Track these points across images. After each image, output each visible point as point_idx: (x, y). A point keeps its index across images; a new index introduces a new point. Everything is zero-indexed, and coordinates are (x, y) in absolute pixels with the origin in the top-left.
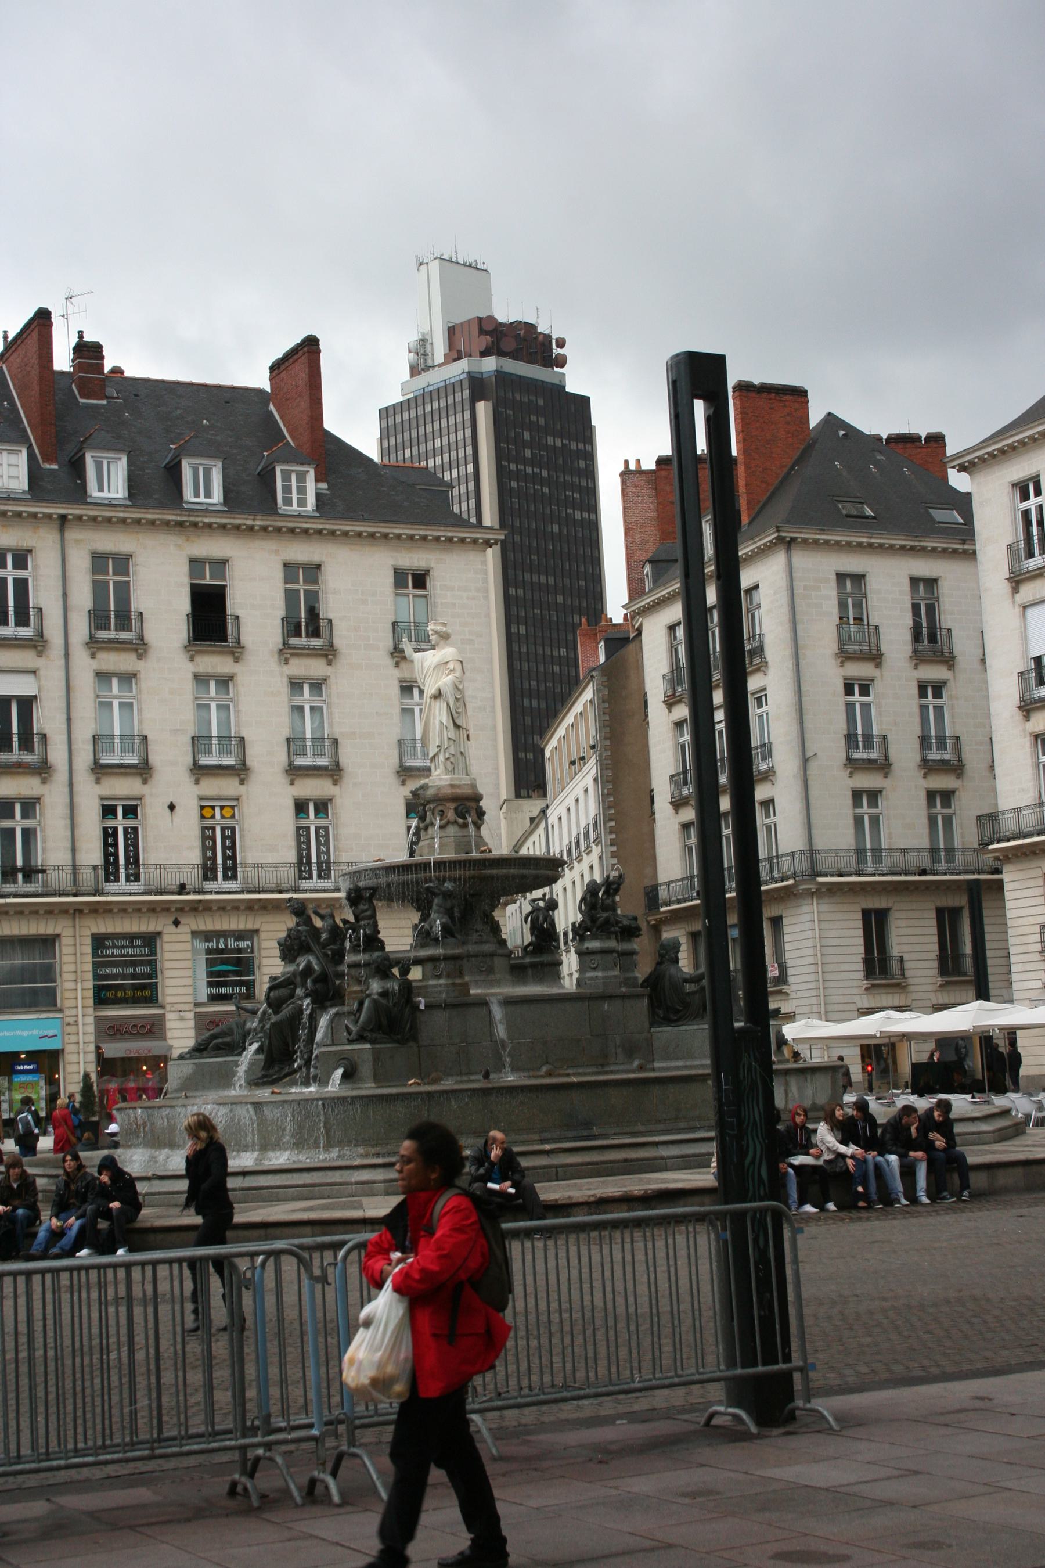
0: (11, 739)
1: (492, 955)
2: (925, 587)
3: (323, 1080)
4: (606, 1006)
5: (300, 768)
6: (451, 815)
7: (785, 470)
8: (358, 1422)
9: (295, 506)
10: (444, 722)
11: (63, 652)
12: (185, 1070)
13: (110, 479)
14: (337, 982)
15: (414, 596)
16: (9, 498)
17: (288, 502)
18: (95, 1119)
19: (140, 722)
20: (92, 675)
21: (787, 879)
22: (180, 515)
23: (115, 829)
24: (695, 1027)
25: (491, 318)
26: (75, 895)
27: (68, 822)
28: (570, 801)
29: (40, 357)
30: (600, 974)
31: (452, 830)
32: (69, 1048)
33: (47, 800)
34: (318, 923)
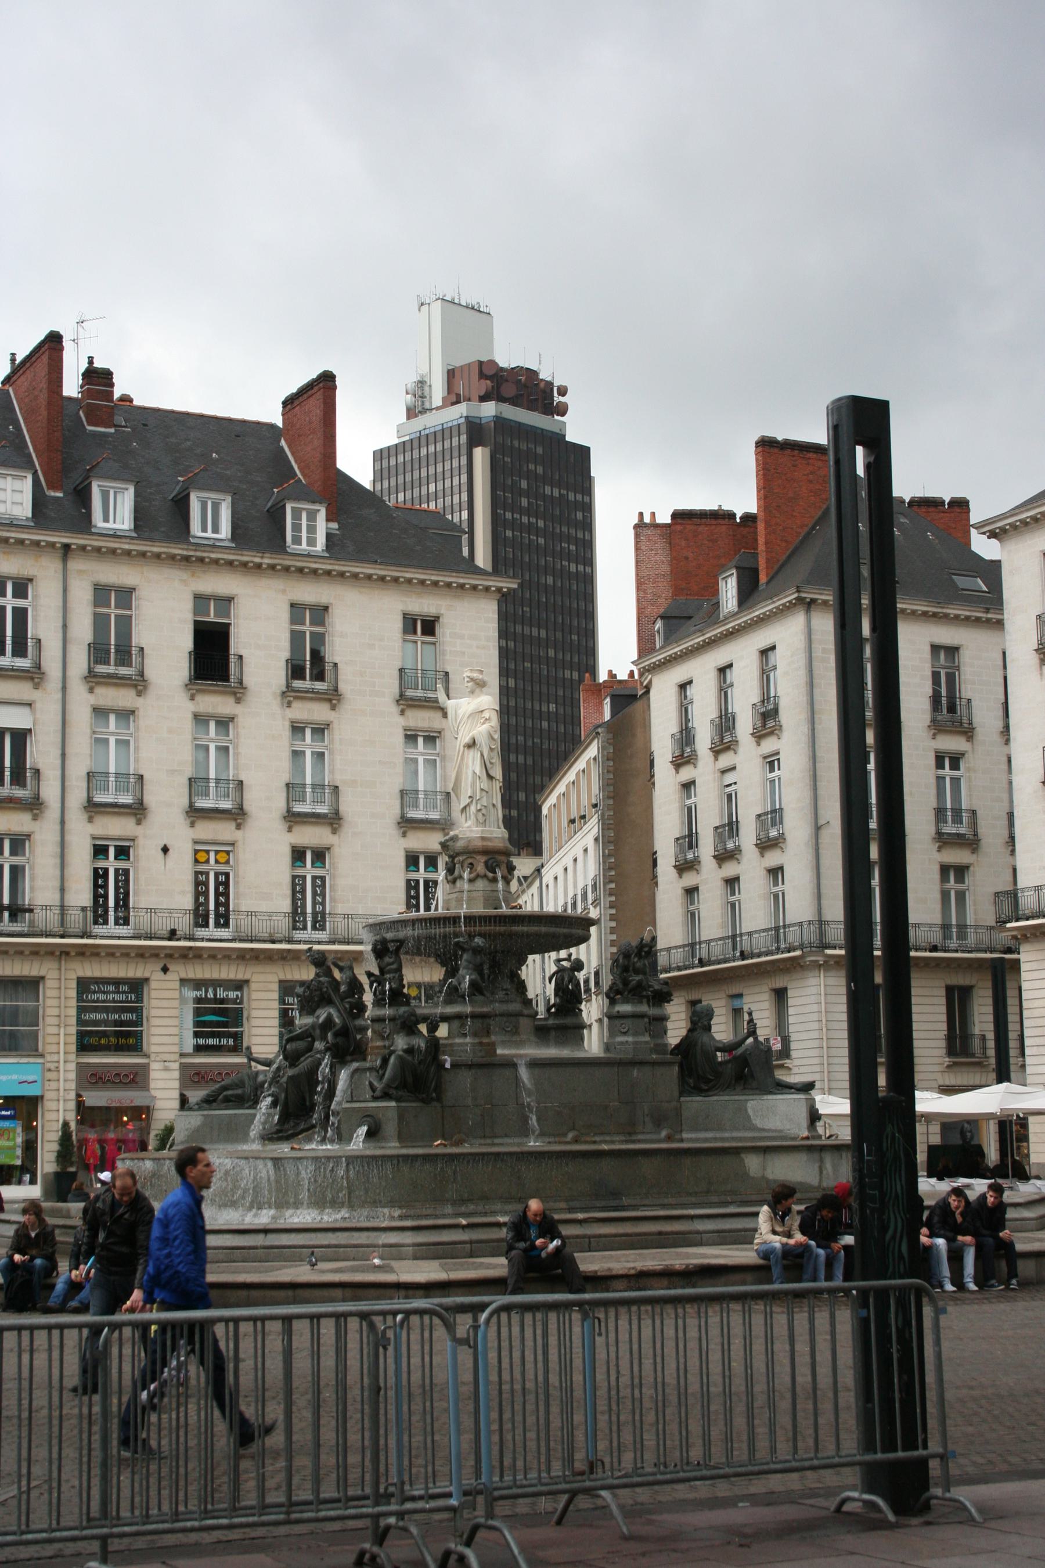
0: (3, 772)
1: (519, 1014)
2: (946, 654)
3: (342, 1136)
4: (635, 1072)
5: (299, 815)
6: (480, 868)
7: (806, 529)
8: (496, 1493)
9: (304, 545)
10: (478, 771)
11: (60, 685)
12: (192, 1121)
13: (116, 509)
14: (358, 1037)
15: (423, 643)
16: (12, 524)
17: (297, 540)
18: (73, 1169)
19: (137, 760)
20: (89, 710)
21: (794, 950)
22: (187, 549)
23: (106, 871)
24: (727, 1098)
25: (492, 363)
26: (62, 937)
27: (58, 861)
28: (568, 861)
29: (50, 381)
30: (630, 1039)
31: (480, 884)
32: (48, 1095)
33: (37, 837)
34: (337, 974)
